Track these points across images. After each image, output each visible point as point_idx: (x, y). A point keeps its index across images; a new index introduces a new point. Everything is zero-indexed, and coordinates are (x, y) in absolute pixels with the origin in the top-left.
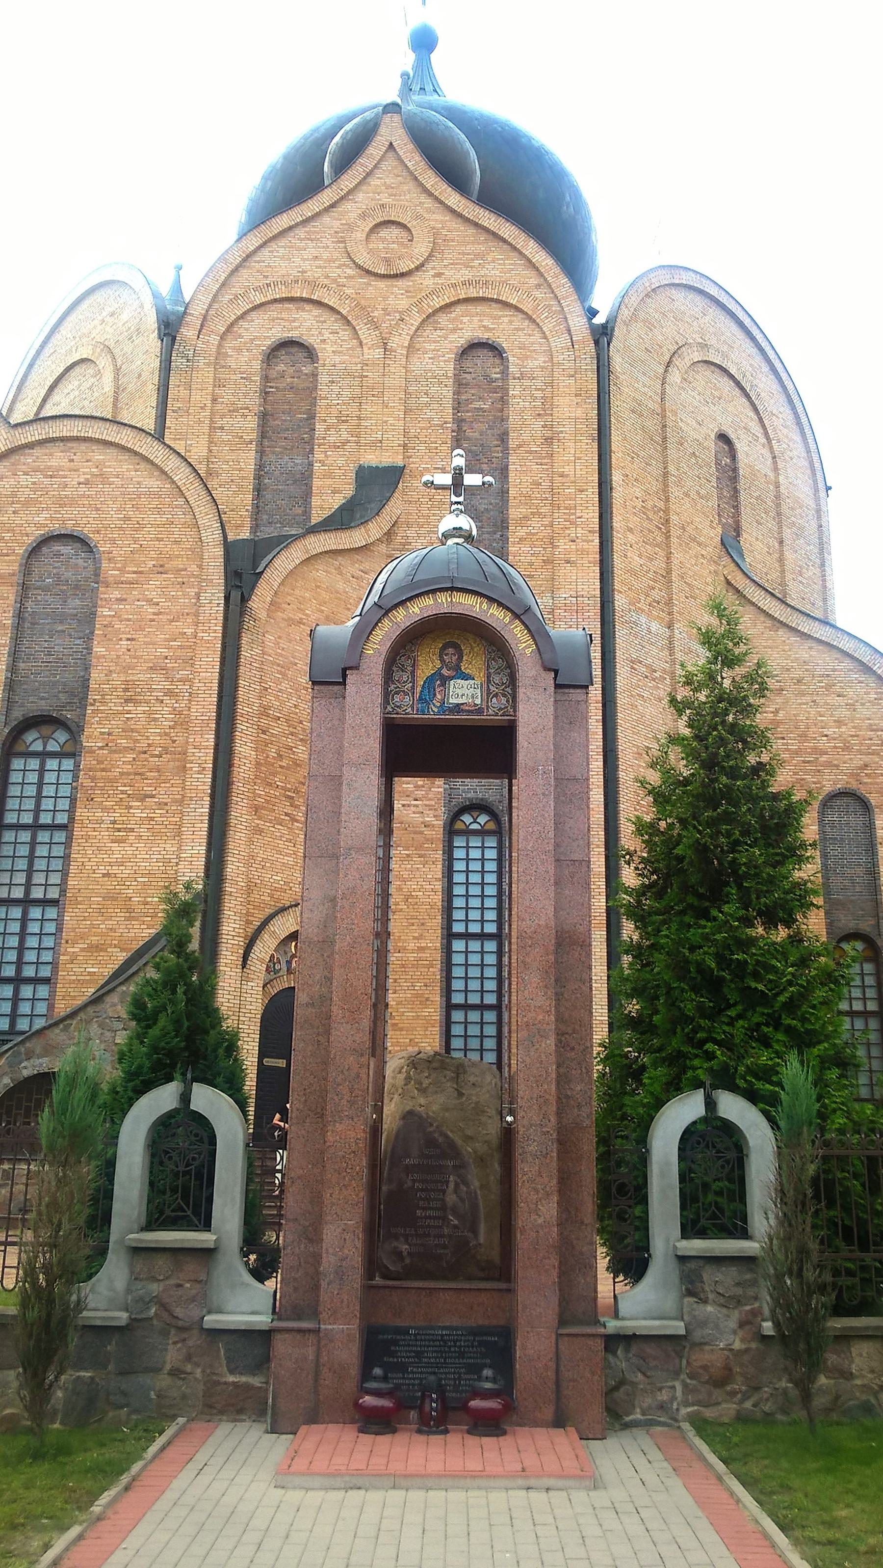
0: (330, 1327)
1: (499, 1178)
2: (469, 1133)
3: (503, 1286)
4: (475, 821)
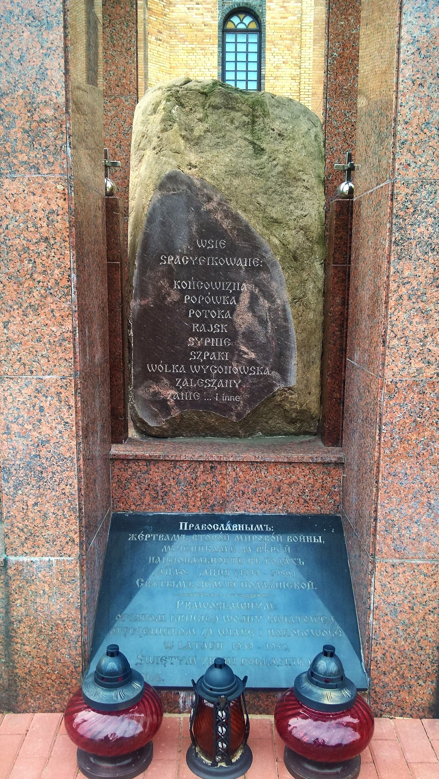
0: (26, 559)
1: (320, 285)
2: (274, 212)
3: (332, 454)
4: (241, 22)
